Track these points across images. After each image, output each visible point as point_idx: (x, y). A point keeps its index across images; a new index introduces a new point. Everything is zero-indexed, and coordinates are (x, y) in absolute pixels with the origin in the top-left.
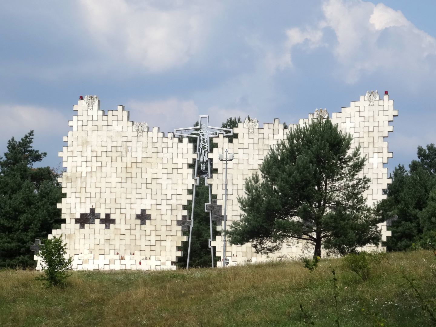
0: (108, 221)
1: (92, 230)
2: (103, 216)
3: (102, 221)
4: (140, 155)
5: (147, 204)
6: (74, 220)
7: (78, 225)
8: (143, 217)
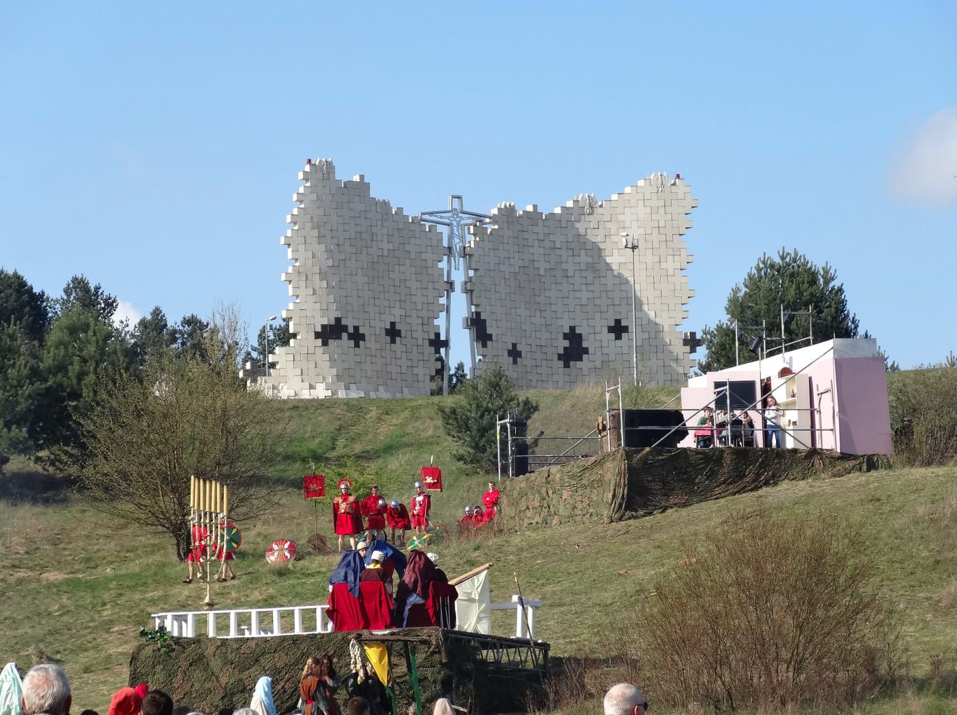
0: (357, 337)
1: (304, 348)
2: (351, 330)
3: (351, 337)
4: (386, 246)
5: (396, 315)
6: (313, 334)
7: (319, 341)
8: (393, 333)
